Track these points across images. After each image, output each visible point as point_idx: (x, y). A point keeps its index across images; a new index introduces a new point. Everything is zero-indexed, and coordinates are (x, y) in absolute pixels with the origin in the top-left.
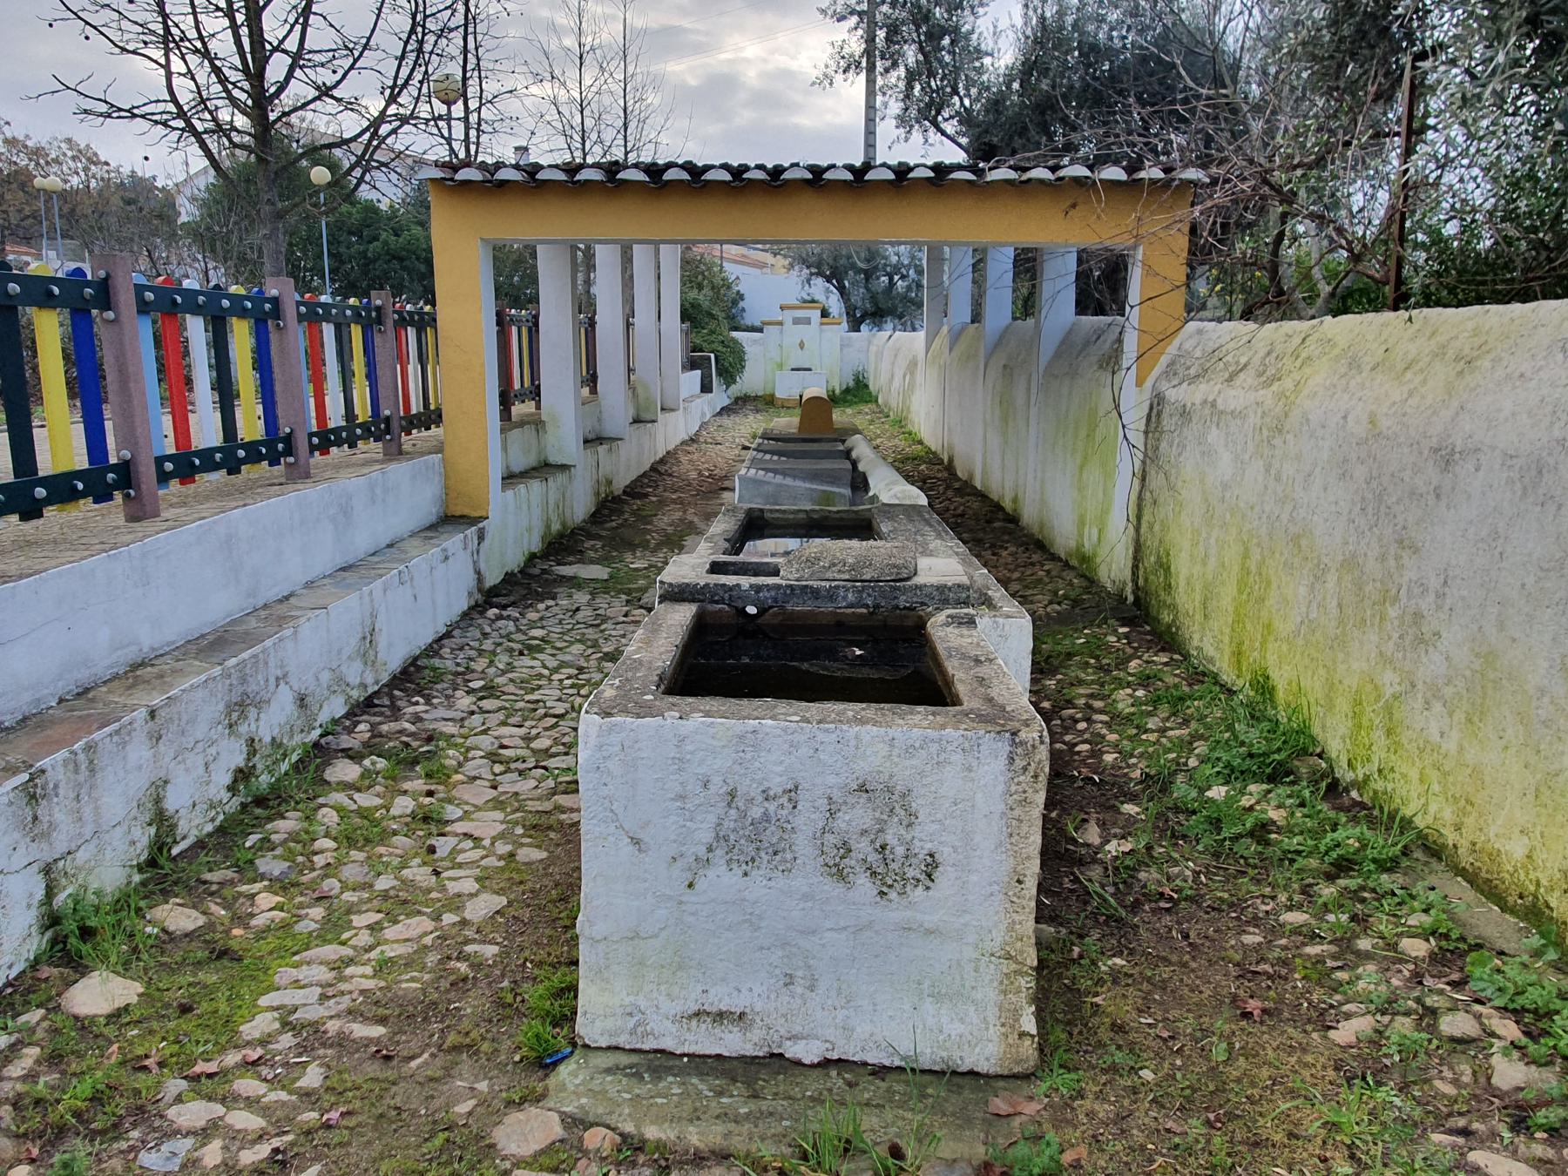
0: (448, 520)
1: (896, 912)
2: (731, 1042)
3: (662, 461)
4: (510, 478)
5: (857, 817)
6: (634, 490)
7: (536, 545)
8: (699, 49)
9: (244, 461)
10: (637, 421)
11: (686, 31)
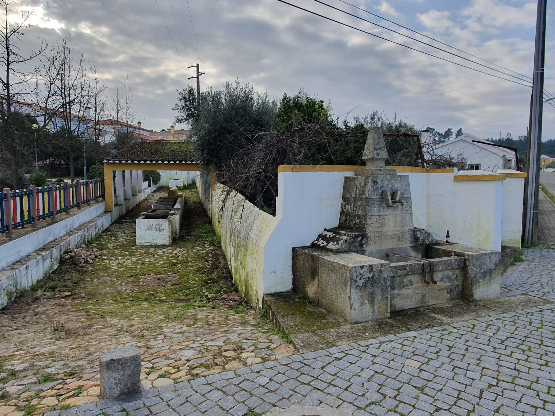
0: (106, 212)
1: (161, 233)
2: (148, 244)
3: (139, 204)
5: (157, 226)
6: (133, 209)
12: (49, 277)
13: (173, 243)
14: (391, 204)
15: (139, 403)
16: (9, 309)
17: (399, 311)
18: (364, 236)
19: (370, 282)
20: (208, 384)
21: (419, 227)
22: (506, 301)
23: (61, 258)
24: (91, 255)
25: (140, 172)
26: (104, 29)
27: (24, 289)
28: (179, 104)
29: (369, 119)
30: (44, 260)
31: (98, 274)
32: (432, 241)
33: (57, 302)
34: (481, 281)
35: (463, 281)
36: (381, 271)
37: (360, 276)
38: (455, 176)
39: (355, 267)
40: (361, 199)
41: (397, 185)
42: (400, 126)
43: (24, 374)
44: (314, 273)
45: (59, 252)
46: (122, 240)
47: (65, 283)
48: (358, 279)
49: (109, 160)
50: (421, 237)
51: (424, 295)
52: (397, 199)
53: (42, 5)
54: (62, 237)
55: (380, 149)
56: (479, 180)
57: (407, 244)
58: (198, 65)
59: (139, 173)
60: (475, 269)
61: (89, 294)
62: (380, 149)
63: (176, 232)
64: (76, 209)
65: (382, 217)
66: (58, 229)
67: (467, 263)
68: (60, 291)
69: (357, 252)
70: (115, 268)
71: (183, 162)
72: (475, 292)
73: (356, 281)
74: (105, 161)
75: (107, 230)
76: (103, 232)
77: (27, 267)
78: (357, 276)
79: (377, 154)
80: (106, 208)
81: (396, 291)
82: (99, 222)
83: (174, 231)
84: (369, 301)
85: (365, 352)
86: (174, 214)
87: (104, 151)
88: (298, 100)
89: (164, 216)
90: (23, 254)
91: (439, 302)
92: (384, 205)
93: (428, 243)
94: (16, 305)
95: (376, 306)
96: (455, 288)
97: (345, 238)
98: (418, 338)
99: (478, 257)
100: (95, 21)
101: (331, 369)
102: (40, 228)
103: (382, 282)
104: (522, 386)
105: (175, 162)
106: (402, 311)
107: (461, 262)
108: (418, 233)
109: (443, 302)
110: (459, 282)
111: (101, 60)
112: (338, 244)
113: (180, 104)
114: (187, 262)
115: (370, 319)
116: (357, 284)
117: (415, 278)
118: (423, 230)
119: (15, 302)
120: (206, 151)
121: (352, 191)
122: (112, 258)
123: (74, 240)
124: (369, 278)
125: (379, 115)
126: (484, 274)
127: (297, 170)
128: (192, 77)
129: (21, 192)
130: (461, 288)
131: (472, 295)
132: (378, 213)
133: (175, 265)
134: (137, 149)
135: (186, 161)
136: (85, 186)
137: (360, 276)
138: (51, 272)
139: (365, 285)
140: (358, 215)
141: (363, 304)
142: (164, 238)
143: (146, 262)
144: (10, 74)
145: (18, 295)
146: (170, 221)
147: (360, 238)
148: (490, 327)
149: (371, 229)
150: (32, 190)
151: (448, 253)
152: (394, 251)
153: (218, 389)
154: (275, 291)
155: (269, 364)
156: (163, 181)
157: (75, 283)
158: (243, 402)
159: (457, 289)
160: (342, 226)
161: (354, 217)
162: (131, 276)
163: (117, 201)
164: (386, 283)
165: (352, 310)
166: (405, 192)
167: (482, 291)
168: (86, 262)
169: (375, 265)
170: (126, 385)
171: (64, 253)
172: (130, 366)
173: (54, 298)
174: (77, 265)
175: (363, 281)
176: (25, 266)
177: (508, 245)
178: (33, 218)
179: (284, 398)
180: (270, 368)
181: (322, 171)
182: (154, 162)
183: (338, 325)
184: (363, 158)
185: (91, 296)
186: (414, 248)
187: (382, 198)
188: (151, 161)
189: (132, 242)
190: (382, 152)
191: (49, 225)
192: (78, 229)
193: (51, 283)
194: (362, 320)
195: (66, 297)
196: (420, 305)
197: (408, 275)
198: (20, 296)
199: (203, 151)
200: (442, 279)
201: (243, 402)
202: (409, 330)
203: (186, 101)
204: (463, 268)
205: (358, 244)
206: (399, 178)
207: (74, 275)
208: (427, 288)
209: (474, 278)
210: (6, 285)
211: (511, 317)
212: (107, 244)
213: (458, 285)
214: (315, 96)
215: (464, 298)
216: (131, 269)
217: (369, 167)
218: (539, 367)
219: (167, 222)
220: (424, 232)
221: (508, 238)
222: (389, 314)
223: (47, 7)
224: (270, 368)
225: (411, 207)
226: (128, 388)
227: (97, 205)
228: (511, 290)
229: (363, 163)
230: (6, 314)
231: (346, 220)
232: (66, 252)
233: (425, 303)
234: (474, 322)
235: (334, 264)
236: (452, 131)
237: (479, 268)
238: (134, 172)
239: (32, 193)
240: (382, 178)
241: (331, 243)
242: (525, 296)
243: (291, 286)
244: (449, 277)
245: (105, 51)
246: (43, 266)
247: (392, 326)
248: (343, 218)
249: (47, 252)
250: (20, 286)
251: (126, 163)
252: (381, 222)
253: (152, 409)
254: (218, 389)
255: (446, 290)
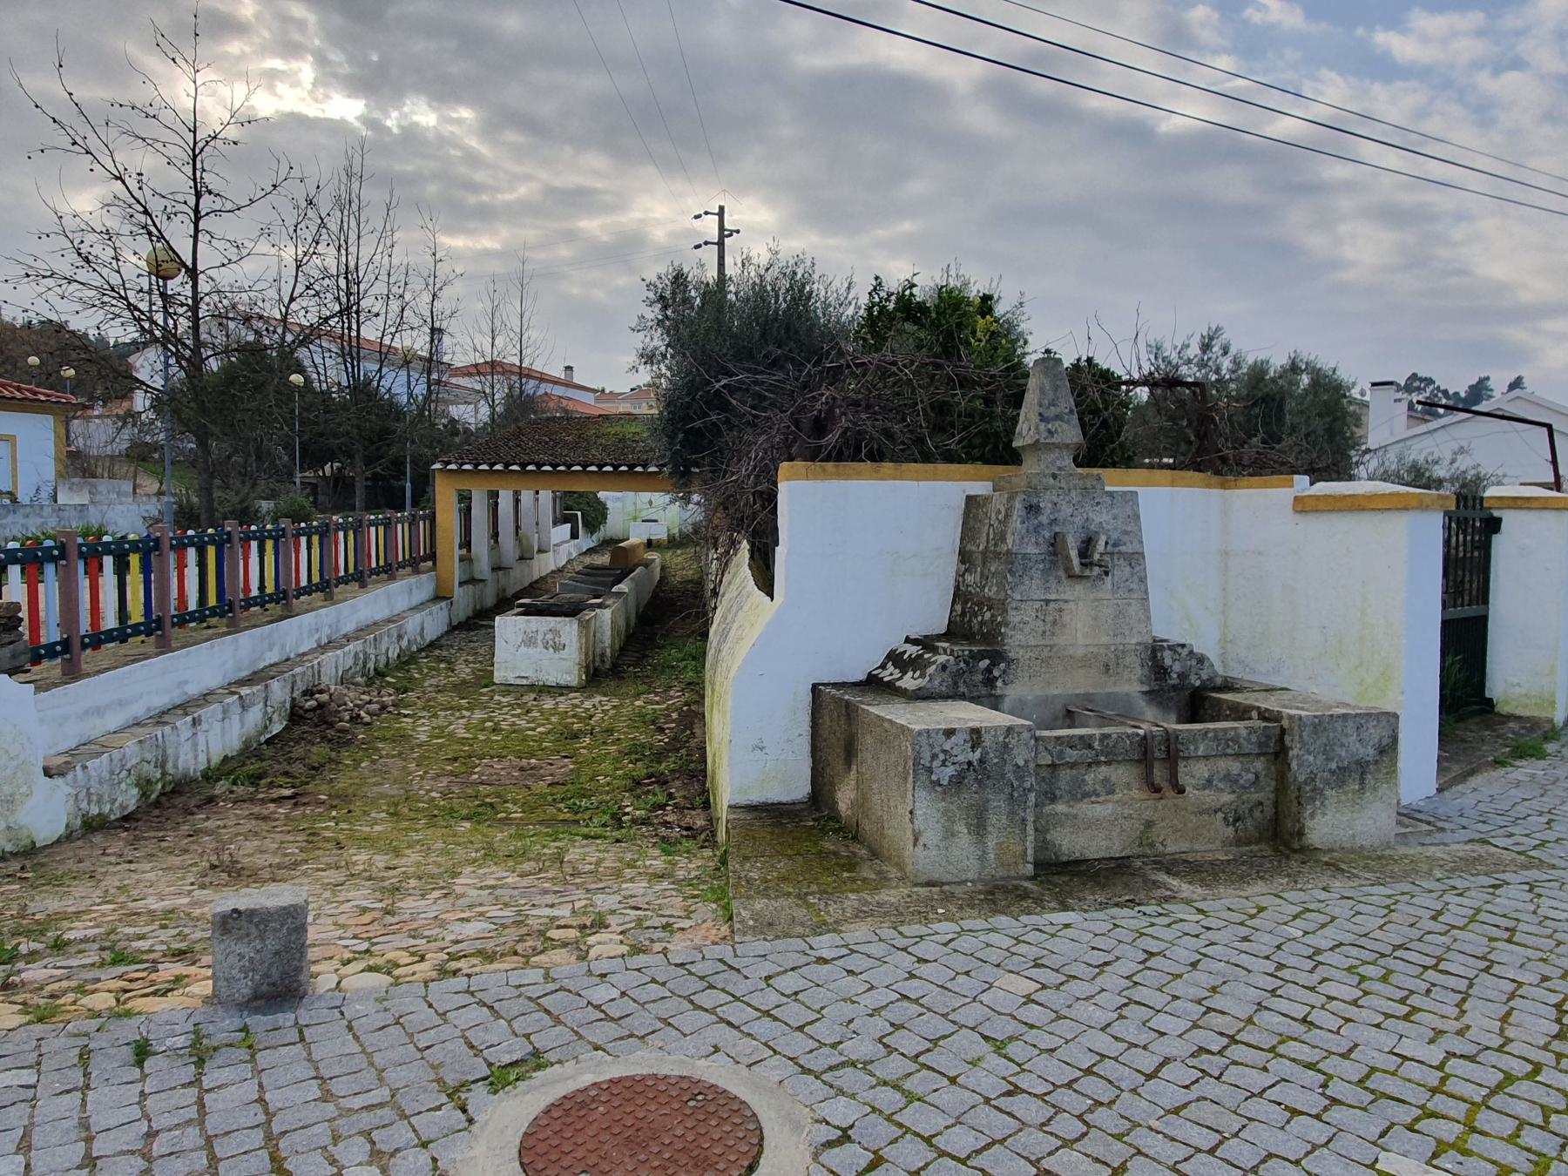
0: (437, 598)
1: (557, 656)
2: (525, 682)
4: (461, 584)
5: (550, 636)
7: (470, 613)
8: (609, 209)
9: (130, 635)
10: (521, 558)
11: (595, 191)
12: (250, 751)
13: (588, 681)
14: (1077, 568)
15: (286, 1018)
16: (138, 820)
17: (1068, 863)
18: (997, 657)
19: (971, 775)
20: (467, 992)
21: (1175, 637)
22: (1406, 856)
23: (293, 706)
24: (370, 702)
25: (546, 496)
26: (465, 113)
27: (185, 776)
28: (650, 316)
29: (1194, 351)
30: (244, 708)
31: (377, 749)
32: (1211, 679)
33: (256, 810)
34: (1328, 793)
35: (1276, 791)
36: (1006, 745)
37: (942, 756)
38: (1296, 498)
39: (928, 731)
40: (997, 555)
41: (1101, 517)
42: (1294, 368)
43: (82, 946)
44: (850, 752)
45: (288, 690)
46: (464, 671)
47: (288, 768)
48: (935, 764)
49: (449, 463)
50: (1177, 667)
51: (1149, 824)
52: (1096, 557)
53: (311, 58)
54: (304, 654)
55: (1058, 417)
56: (1362, 509)
57: (1132, 684)
58: (722, 209)
59: (540, 501)
60: (1311, 758)
61: (338, 797)
62: (1058, 417)
63: (603, 655)
64: (355, 586)
65: (1052, 605)
66: (296, 633)
67: (1287, 738)
68: (271, 785)
69: (975, 700)
70: (423, 737)
71: (639, 469)
72: (1309, 823)
73: (930, 770)
74: (438, 466)
75: (433, 645)
76: (420, 650)
77: (195, 722)
78: (934, 757)
79: (1049, 431)
80: (438, 587)
81: (1060, 808)
82: (412, 624)
83: (598, 651)
84: (968, 825)
85: (904, 950)
86: (600, 606)
87: (454, 441)
88: (912, 294)
89: (572, 610)
90: (194, 690)
91: (1197, 847)
92: (1061, 573)
93: (1198, 683)
94: (157, 812)
95: (991, 842)
96: (1251, 810)
97: (942, 659)
98: (1077, 930)
99: (1320, 725)
100: (443, 91)
101: (788, 983)
102: (247, 628)
103: (1010, 776)
104: (1294, 1060)
105: (616, 467)
106: (1077, 862)
107: (1268, 737)
108: (1167, 653)
109: (1213, 847)
110: (1265, 795)
111: (472, 199)
112: (922, 676)
113: (652, 316)
114: (610, 731)
115: (970, 876)
116: (934, 777)
117: (1122, 774)
118: (1183, 646)
119: (157, 804)
120: (681, 436)
121: (980, 533)
122: (424, 713)
123: (332, 665)
124: (970, 763)
125: (1224, 338)
126: (1341, 776)
127: (830, 476)
128: (706, 243)
129: (200, 536)
130: (1269, 810)
131: (1300, 833)
132: (1040, 594)
133: (575, 736)
134: (541, 435)
135: (644, 466)
136: (381, 529)
137: (942, 756)
138: (263, 739)
139: (958, 781)
140: (990, 599)
141: (950, 834)
142: (564, 667)
143: (504, 725)
144: (200, 245)
145: (168, 789)
146: (584, 625)
147: (987, 662)
148: (1307, 915)
149: (1019, 638)
150: (229, 533)
151: (1240, 712)
152: (1090, 701)
153: (484, 1005)
154: (762, 800)
155: (641, 960)
156: (614, 524)
157: (314, 768)
158: (527, 1036)
159: (1257, 814)
160: (955, 632)
161: (980, 604)
162: (455, 759)
163: (471, 571)
164: (1021, 779)
165: (919, 848)
166: (1125, 538)
167: (1326, 824)
168: (355, 719)
169: (988, 729)
170: (267, 975)
171: (305, 693)
172: (275, 930)
173: (251, 800)
174: (331, 725)
175: (950, 770)
176: (189, 718)
177: (1518, 712)
178: (231, 604)
179: (631, 1036)
180: (639, 970)
181: (901, 479)
182: (562, 468)
183: (882, 881)
184: (1014, 445)
185: (342, 799)
186: (1153, 696)
187: (1055, 554)
188: (554, 466)
189: (485, 678)
190: (1065, 426)
191: (272, 622)
192: (348, 638)
193: (251, 769)
194: (949, 878)
195: (280, 800)
196: (1138, 850)
197: (1098, 763)
198: (173, 791)
199: (672, 437)
200: (1209, 781)
201: (527, 1036)
202: (1065, 908)
203: (665, 307)
204: (1276, 754)
205: (980, 677)
206: (1107, 499)
207: (314, 749)
208: (1160, 805)
209: (1305, 783)
210: (134, 762)
211: (1389, 897)
212: (424, 680)
213: (1261, 803)
214: (994, 284)
215: (1274, 837)
216: (463, 741)
217: (1031, 467)
218: (1380, 1019)
219: (575, 626)
220: (1184, 652)
221: (1518, 690)
222: (1030, 867)
223: (321, 61)
224: (639, 970)
225: (1143, 580)
226: (274, 985)
227: (413, 580)
228: (1442, 830)
229: (1012, 457)
230: (127, 830)
231: (963, 613)
232: (308, 693)
233: (1152, 845)
234: (1264, 901)
235: (886, 725)
236: (1491, 384)
237: (1321, 757)
238: (526, 496)
239: (229, 540)
240: (1054, 498)
241: (910, 674)
242: (1477, 847)
243: (808, 789)
244: (1228, 777)
245: (480, 176)
246: (242, 721)
247: (1025, 895)
248: (958, 608)
249: (255, 689)
250: (175, 767)
251: (491, 472)
252: (1049, 619)
253: (307, 1032)
254: (484, 1005)
255: (1220, 815)
